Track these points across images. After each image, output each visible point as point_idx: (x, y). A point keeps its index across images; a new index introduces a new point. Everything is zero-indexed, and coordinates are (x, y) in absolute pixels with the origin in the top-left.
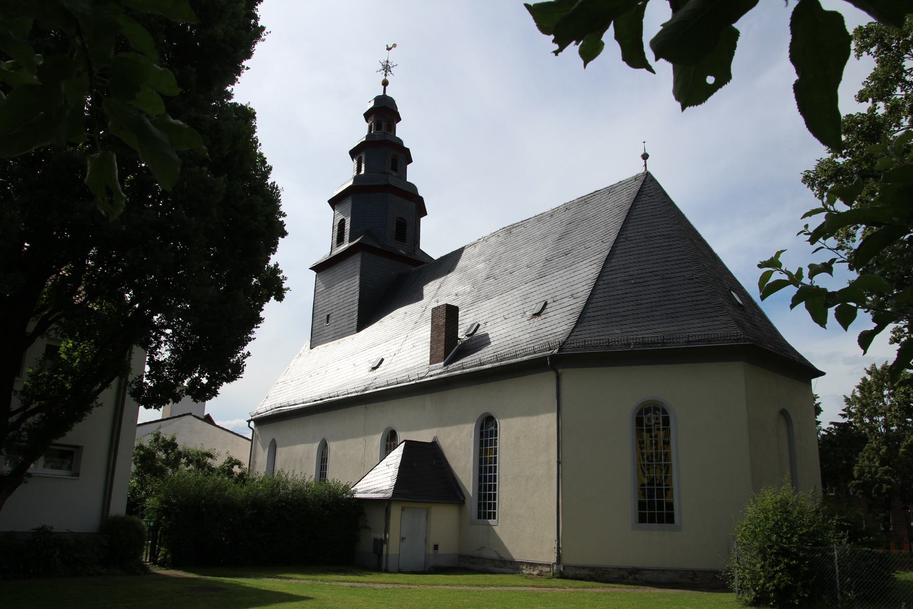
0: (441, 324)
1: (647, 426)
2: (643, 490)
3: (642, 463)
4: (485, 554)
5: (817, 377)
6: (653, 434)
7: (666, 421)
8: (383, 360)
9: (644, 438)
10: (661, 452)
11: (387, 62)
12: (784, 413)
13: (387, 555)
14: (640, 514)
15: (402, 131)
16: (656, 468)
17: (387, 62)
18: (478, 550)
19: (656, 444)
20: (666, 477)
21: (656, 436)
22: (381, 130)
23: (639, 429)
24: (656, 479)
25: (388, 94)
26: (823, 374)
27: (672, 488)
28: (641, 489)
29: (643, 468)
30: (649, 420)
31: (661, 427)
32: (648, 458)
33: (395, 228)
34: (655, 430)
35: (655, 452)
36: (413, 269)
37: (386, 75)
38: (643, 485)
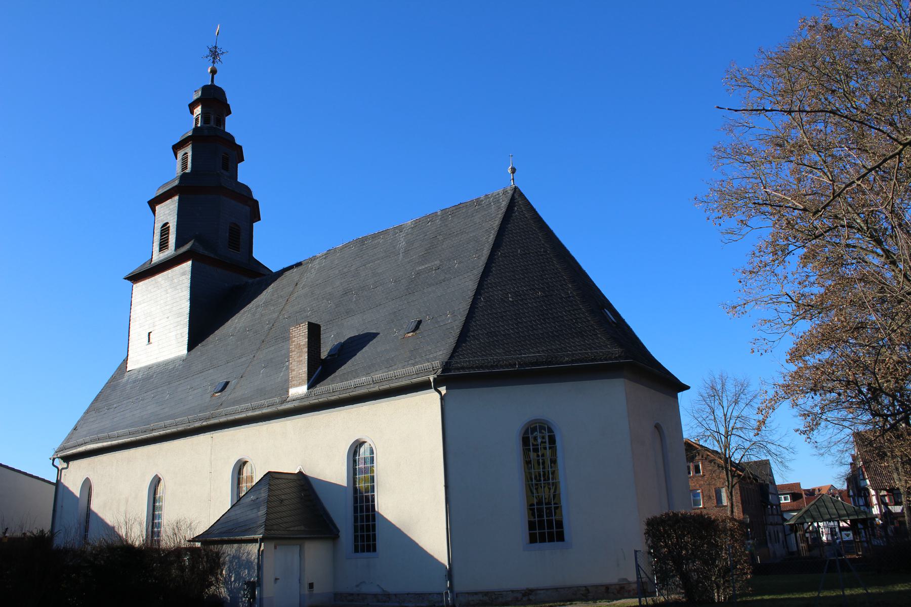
0: (302, 344)
1: (533, 445)
2: (532, 510)
3: (530, 483)
4: (365, 589)
5: (682, 391)
6: (540, 454)
7: (552, 440)
8: (227, 383)
9: (531, 457)
10: (548, 472)
12: (658, 427)
13: (261, 599)
14: (530, 534)
15: (231, 125)
16: (544, 487)
17: (216, 47)
18: (357, 586)
19: (543, 463)
20: (554, 497)
21: (543, 455)
22: (209, 124)
23: (526, 449)
24: (545, 499)
25: (216, 83)
26: (687, 388)
27: (561, 506)
28: (531, 509)
29: (532, 488)
30: (535, 439)
31: (548, 445)
32: (536, 478)
33: (227, 235)
34: (542, 448)
35: (543, 471)
36: (250, 281)
37: (214, 62)
38: (532, 505)
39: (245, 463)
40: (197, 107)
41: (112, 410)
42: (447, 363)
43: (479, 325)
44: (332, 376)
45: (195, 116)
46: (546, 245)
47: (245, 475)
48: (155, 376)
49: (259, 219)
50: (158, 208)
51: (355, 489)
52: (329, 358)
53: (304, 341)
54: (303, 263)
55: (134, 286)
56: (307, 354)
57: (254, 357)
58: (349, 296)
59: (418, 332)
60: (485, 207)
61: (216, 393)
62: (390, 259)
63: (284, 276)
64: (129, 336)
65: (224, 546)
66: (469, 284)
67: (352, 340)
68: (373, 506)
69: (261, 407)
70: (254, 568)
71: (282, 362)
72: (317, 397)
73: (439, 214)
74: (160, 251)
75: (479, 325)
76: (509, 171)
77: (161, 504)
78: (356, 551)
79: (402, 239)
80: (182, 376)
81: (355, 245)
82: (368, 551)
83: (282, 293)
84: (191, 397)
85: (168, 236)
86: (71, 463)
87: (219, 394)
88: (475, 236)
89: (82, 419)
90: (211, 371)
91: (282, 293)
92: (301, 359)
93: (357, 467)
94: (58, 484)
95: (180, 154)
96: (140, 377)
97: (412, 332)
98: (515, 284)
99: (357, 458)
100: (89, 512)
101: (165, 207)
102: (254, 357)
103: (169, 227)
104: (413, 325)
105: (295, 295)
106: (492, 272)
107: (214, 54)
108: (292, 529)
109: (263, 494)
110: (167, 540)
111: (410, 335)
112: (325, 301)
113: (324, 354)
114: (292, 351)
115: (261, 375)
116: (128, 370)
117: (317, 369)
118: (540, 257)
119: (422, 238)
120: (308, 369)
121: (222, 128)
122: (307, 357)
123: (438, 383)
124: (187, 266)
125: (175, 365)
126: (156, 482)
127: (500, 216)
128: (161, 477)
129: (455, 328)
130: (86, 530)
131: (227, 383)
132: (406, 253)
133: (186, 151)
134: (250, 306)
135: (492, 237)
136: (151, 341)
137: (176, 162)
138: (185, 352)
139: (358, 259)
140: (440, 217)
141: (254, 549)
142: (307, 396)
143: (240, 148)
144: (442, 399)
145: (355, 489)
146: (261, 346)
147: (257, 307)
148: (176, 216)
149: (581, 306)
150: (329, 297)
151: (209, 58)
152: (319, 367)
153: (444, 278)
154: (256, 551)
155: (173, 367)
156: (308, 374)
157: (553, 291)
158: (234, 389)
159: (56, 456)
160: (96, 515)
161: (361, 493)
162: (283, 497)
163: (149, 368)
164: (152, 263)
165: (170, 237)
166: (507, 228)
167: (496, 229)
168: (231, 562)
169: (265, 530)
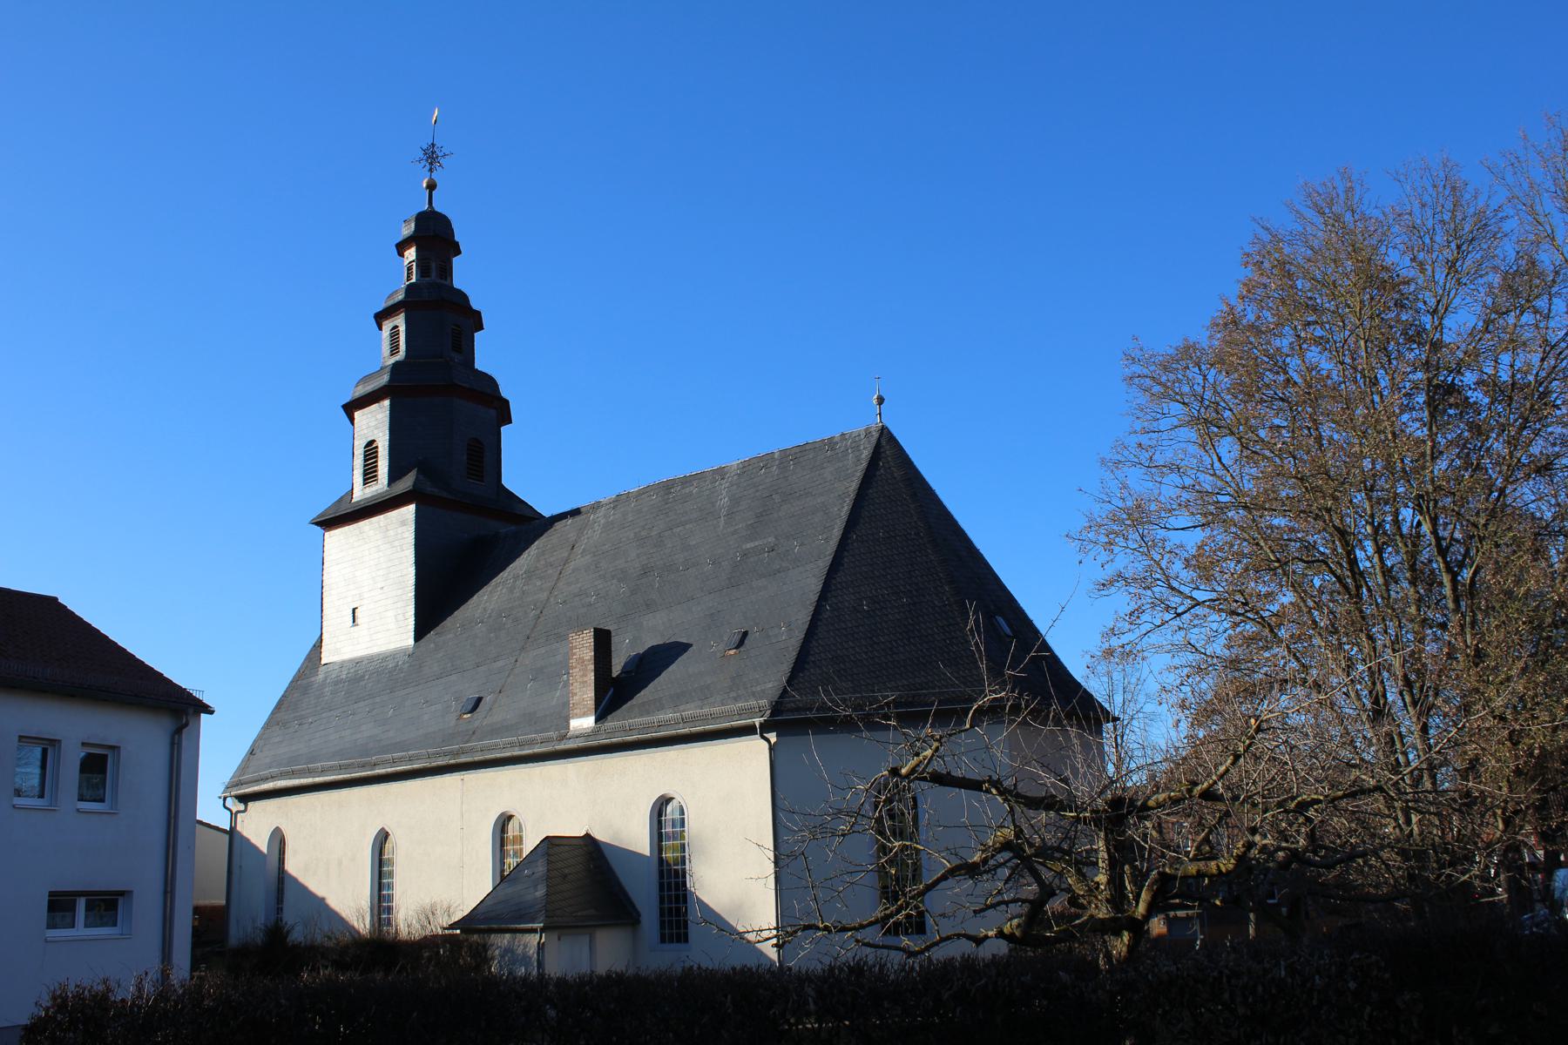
8: (479, 700)
11: (433, 145)
17: (433, 145)
22: (429, 276)
25: (438, 208)
33: (465, 457)
37: (431, 170)
39: (510, 817)
40: (408, 249)
41: (306, 726)
42: (776, 702)
43: (822, 646)
44: (629, 704)
45: (406, 262)
46: (919, 523)
47: (510, 834)
48: (367, 677)
49: (511, 422)
50: (357, 415)
51: (661, 860)
52: (623, 675)
53: (589, 654)
54: (582, 510)
55: (327, 534)
56: (593, 674)
57: (516, 661)
58: (651, 578)
59: (742, 649)
60: (840, 455)
61: (464, 714)
62: (707, 524)
63: (552, 529)
64: (322, 611)
65: (493, 936)
66: (814, 585)
67: (654, 650)
68: (684, 884)
69: (532, 743)
70: (532, 965)
71: (555, 675)
72: (609, 735)
73: (776, 456)
74: (364, 484)
75: (822, 646)
76: (875, 402)
77: (390, 868)
78: (663, 940)
79: (724, 492)
80: (411, 681)
81: (657, 491)
82: (679, 941)
83: (552, 559)
84: (426, 717)
85: (376, 462)
86: (250, 804)
87: (469, 715)
88: (823, 503)
89: (260, 737)
90: (453, 677)
91: (552, 559)
92: (585, 679)
93: (663, 831)
94: (232, 833)
95: (387, 326)
96: (344, 677)
97: (736, 648)
98: (873, 584)
99: (663, 818)
100: (282, 876)
101: (369, 416)
102: (516, 661)
103: (377, 447)
104: (737, 638)
105: (572, 565)
106: (843, 565)
107: (432, 157)
108: (579, 914)
109: (541, 868)
110: (408, 918)
111: (732, 652)
112: (615, 581)
113: (615, 672)
114: (573, 668)
115: (529, 692)
116: (323, 662)
117: (607, 693)
118: (910, 542)
119: (752, 496)
120: (595, 694)
121: (448, 283)
122: (593, 678)
123: (766, 728)
124: (409, 511)
125: (398, 662)
126: (383, 838)
127: (859, 474)
128: (390, 833)
129: (791, 649)
130: (278, 899)
131: (479, 700)
132: (729, 516)
133: (396, 323)
134: (504, 574)
135: (846, 508)
136: (357, 621)
137: (381, 335)
138: (411, 642)
139: (662, 517)
140: (777, 462)
141: (533, 939)
142: (594, 733)
143: (479, 313)
144: (772, 748)
145: (661, 860)
146: (526, 644)
147: (516, 577)
148: (387, 432)
149: (959, 619)
150: (621, 576)
151: (423, 163)
152: (610, 690)
153: (778, 567)
154: (536, 943)
155: (393, 665)
156: (595, 701)
157: (924, 596)
158: (491, 709)
159: (227, 794)
160: (295, 881)
161: (669, 865)
162: (566, 871)
163: (357, 662)
164: (354, 501)
165: (380, 463)
166: (821, 620)
167: (853, 496)
168: (502, 956)
169: (546, 917)
